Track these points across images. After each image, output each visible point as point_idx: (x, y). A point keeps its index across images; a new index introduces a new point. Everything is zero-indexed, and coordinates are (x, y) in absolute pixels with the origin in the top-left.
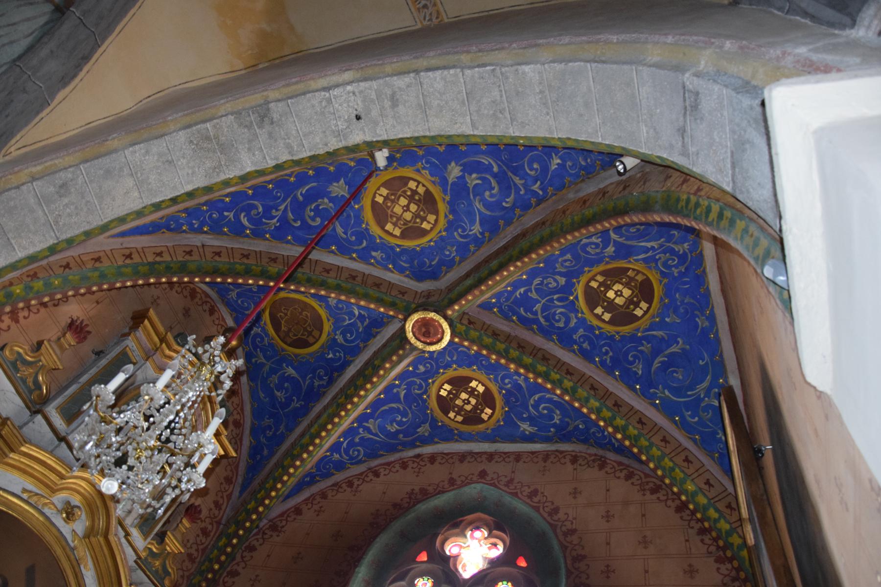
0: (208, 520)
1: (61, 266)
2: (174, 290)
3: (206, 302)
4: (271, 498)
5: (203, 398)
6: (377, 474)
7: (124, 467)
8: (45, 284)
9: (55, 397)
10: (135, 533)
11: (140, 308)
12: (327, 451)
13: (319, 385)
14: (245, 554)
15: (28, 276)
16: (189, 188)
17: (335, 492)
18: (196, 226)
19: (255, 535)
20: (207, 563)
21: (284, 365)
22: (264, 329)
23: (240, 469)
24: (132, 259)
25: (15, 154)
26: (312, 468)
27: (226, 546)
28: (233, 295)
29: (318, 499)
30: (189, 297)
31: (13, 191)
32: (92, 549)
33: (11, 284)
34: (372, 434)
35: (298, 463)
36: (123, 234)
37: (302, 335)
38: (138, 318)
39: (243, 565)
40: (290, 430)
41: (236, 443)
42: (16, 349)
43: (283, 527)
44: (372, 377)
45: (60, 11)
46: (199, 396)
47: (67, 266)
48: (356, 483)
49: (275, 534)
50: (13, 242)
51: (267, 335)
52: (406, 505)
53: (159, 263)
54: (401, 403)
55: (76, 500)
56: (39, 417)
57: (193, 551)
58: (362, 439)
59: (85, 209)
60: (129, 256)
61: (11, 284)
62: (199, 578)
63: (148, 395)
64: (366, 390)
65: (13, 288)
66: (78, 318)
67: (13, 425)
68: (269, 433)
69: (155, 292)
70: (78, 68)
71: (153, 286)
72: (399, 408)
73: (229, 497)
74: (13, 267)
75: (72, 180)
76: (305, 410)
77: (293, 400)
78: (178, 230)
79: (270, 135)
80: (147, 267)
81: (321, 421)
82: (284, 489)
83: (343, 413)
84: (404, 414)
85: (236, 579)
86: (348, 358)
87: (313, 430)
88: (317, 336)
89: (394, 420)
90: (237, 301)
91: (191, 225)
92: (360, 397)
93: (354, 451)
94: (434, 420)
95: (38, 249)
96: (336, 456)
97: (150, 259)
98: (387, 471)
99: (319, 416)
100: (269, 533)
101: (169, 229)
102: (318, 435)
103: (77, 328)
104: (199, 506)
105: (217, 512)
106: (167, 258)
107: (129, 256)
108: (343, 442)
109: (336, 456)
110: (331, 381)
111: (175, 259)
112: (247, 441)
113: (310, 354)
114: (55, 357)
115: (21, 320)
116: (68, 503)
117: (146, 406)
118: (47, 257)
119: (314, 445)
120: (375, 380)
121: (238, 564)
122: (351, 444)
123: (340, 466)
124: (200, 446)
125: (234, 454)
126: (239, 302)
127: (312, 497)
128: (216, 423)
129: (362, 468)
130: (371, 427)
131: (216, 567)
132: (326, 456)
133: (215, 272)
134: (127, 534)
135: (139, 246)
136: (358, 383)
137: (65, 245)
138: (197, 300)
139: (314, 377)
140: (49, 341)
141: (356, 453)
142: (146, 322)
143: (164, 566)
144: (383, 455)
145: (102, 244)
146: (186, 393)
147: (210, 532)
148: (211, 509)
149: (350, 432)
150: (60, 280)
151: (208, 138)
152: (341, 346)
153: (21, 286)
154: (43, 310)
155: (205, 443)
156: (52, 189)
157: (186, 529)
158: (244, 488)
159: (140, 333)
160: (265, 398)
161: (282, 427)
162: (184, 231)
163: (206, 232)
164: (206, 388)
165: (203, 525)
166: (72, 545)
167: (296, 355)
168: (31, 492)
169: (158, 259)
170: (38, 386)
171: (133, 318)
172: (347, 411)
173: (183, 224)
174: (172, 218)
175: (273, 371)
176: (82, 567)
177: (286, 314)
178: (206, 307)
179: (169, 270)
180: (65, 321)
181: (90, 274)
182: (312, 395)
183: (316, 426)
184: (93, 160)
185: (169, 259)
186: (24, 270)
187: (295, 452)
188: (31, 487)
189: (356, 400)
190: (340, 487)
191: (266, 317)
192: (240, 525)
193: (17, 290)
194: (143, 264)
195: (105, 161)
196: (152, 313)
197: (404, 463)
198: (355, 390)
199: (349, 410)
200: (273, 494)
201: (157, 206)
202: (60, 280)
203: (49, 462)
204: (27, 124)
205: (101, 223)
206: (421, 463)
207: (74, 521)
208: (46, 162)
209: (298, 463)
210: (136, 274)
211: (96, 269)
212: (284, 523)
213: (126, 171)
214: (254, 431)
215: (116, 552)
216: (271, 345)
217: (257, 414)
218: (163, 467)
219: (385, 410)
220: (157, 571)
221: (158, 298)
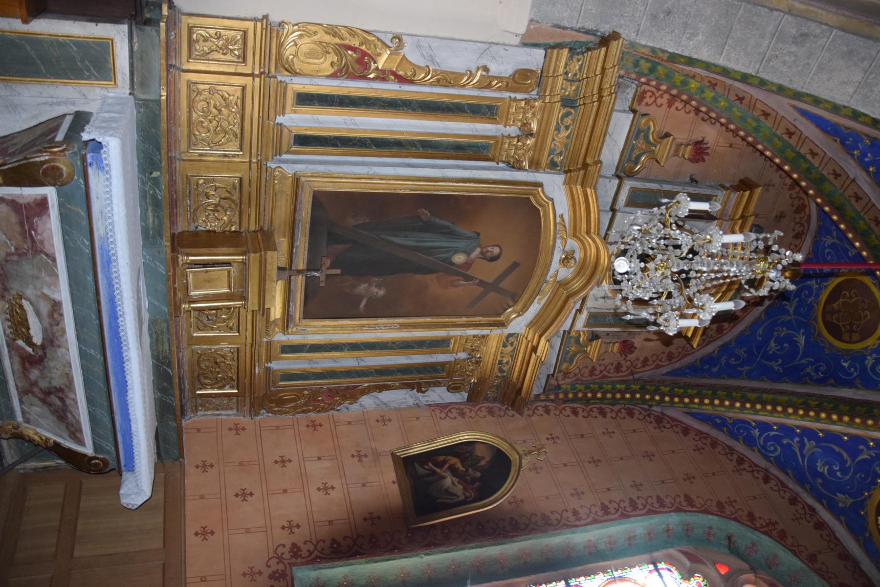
0: (628, 363)
1: (737, 95)
2: (790, 192)
3: (802, 225)
4: (682, 401)
5: (732, 283)
6: (766, 480)
7: (642, 265)
8: (714, 98)
9: (638, 180)
10: (584, 316)
11: (754, 179)
12: (755, 421)
13: (808, 374)
14: (623, 411)
15: (709, 82)
17: (723, 452)
18: (866, 159)
19: (642, 408)
20: (596, 386)
21: (803, 330)
22: (820, 289)
23: (686, 359)
24: (790, 137)
26: (730, 418)
27: (620, 391)
28: (829, 241)
29: (708, 441)
30: (794, 208)
31: (766, 10)
32: (555, 294)
34: (801, 452)
35: (727, 403)
36: (804, 113)
37: (844, 326)
38: (745, 185)
39: (614, 415)
40: (749, 376)
41: (704, 340)
42: (651, 123)
43: (665, 427)
44: (858, 416)
46: (736, 276)
47: (741, 99)
48: (746, 466)
49: (654, 424)
50: (727, 47)
51: (818, 296)
52: (758, 525)
53: (806, 160)
54: (853, 461)
55: (578, 256)
56: (617, 181)
57: (598, 368)
58: (789, 446)
59: (800, 69)
60: (790, 134)
61: (693, 77)
62: (582, 387)
63: (711, 236)
64: (840, 419)
65: (692, 81)
66: (707, 143)
67: (599, 171)
68: (733, 361)
69: (776, 178)
71: (781, 172)
72: (846, 461)
73: (658, 367)
74: (707, 66)
75: (815, 36)
76: (777, 377)
77: (777, 361)
78: (848, 150)
80: (794, 155)
81: (780, 398)
82: (696, 406)
83: (801, 412)
84: (844, 471)
85: (600, 417)
86: (858, 381)
87: (765, 396)
88: (855, 338)
89: (830, 465)
90: (826, 248)
91: (864, 155)
92: (829, 417)
93: (772, 445)
94: (862, 504)
95: (737, 68)
96: (756, 432)
97: (802, 151)
98: (776, 488)
99: (782, 393)
100: (652, 419)
101: (843, 143)
102: (764, 404)
103: (700, 150)
104: (636, 348)
105: (639, 365)
106: (816, 162)
107: (790, 134)
108: (773, 430)
109: (756, 432)
110: (822, 382)
111: (820, 169)
112: (710, 349)
113: (831, 345)
114: (666, 153)
115: (673, 107)
116: (574, 252)
117: (701, 242)
118: (735, 79)
119: (753, 406)
120: (858, 420)
121: (612, 410)
122: (777, 439)
123: (750, 442)
124: (702, 308)
125: (695, 346)
126: (827, 250)
127: (706, 436)
128: (728, 306)
129: (763, 463)
130: (807, 446)
131: (599, 395)
132: (749, 424)
133: (838, 209)
134: (580, 311)
135: (806, 133)
136: (841, 407)
137: (756, 82)
138: (798, 216)
139: (812, 364)
140: (674, 139)
141: (772, 448)
142: (748, 193)
143: (575, 355)
144: (788, 474)
145: (782, 106)
146: (732, 265)
147: (621, 371)
148: (638, 359)
149: (788, 431)
150: (727, 104)
152: (864, 368)
153: (698, 85)
154: (692, 114)
155: (707, 309)
157: (612, 351)
158: (673, 373)
159: (735, 196)
160: (760, 336)
161: (746, 368)
162: (852, 155)
163: (868, 172)
164: (748, 277)
165: (623, 362)
166: (548, 278)
167: (820, 334)
168: (563, 221)
169: (809, 157)
170: (636, 162)
171: (741, 181)
172: (806, 414)
173: (858, 149)
174: (857, 136)
175: (788, 325)
176: (538, 297)
177: (851, 297)
178: (798, 229)
179: (807, 173)
180: (697, 137)
181: (749, 120)
182: (795, 374)
183: (771, 396)
184: (849, 32)
185: (817, 165)
186: (712, 75)
187: (734, 394)
188: (566, 218)
189: (823, 415)
190: (732, 454)
191: (835, 282)
192: (643, 390)
193: (693, 84)
194: (793, 150)
196: (758, 191)
197: (795, 499)
198: (832, 409)
199: (809, 416)
200: (687, 400)
201: (856, 115)
202: (727, 104)
203: (592, 215)
205: (799, 89)
206: (808, 516)
207: (565, 266)
208: (812, 5)
209: (727, 403)
210: (781, 152)
211: (757, 120)
212: (668, 426)
214: (725, 347)
215: (560, 318)
216: (811, 307)
217: (741, 340)
218: (662, 293)
219: (834, 450)
220: (568, 353)
221: (774, 185)
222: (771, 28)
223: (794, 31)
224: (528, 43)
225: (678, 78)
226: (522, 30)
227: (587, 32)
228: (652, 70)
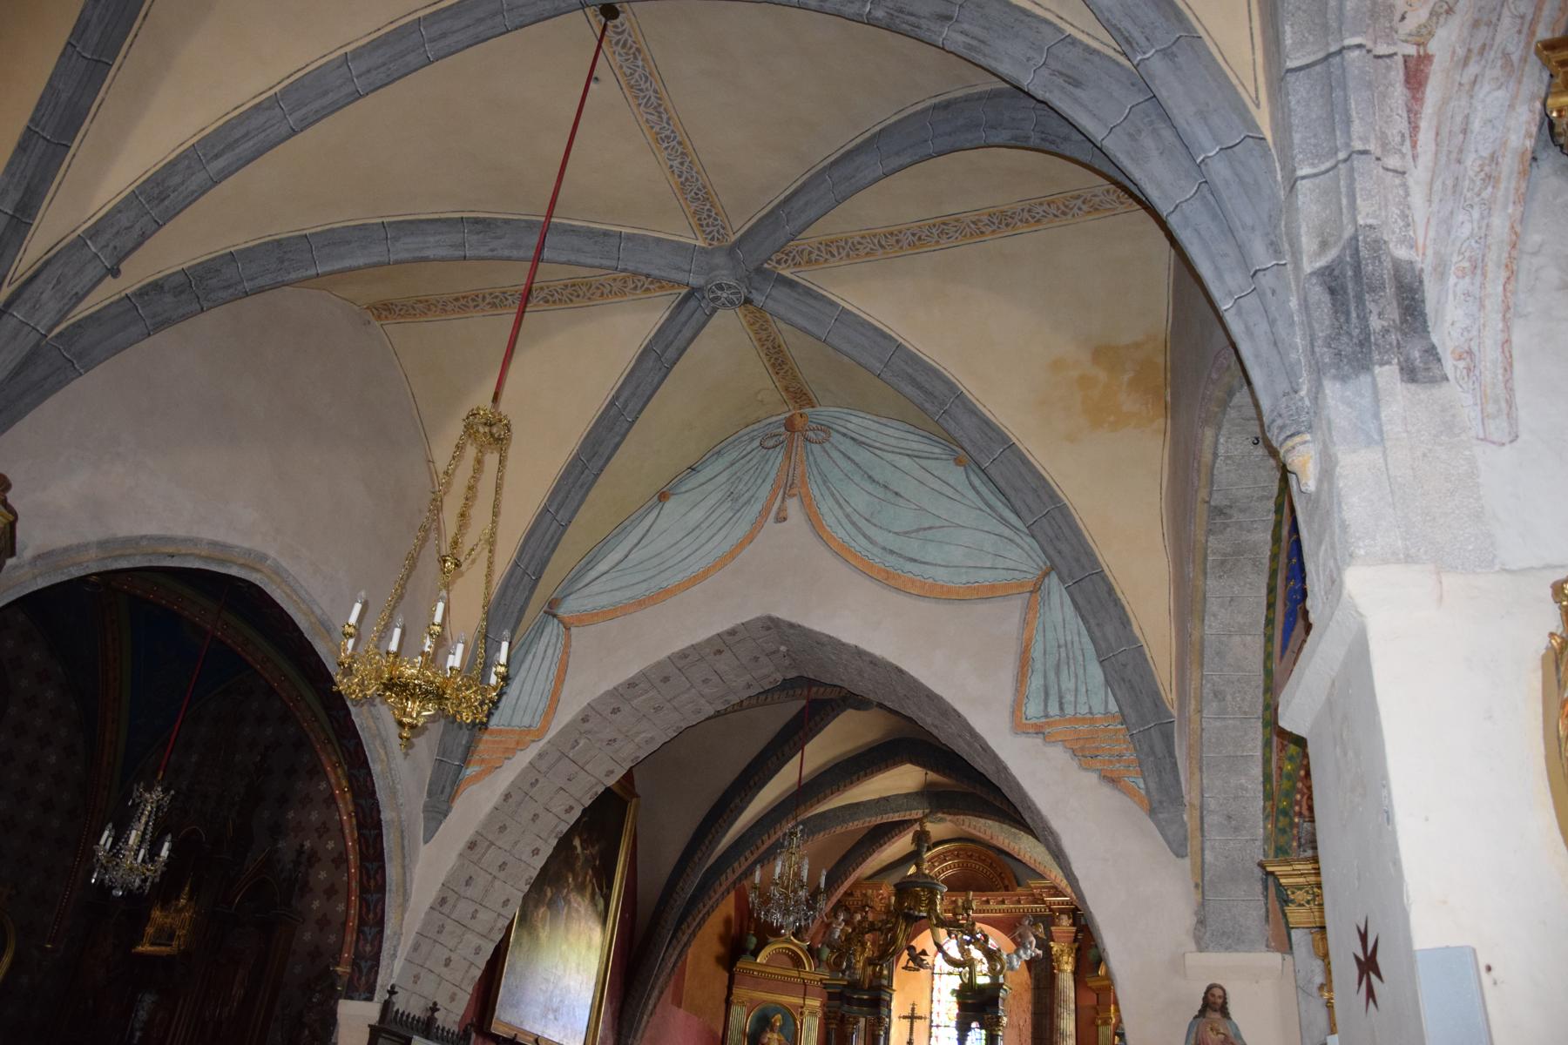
16: (1264, 591)
25: (1174, 696)
33: (1281, 769)
45: (610, 12)
61: (1281, 769)
70: (1117, 602)
79: (1242, 511)
95: (1260, 737)
151: (1223, 563)
156: (1214, 704)
195: (1208, 653)
204: (1152, 675)
213: (1224, 639)
222: (1218, 724)
223: (1214, 704)
224: (1286, 946)
225: (1286, 784)
226: (1278, 956)
227: (1266, 888)
228: (1285, 813)
